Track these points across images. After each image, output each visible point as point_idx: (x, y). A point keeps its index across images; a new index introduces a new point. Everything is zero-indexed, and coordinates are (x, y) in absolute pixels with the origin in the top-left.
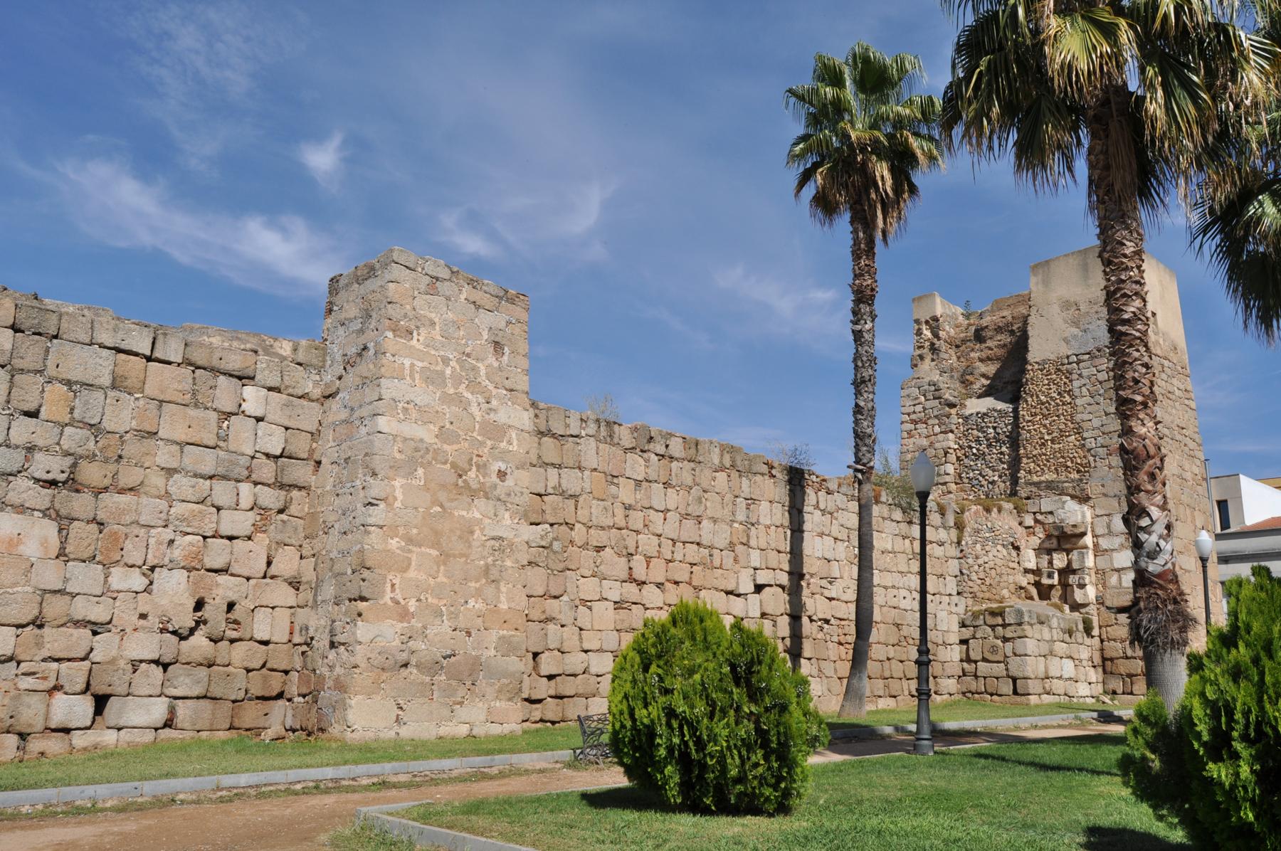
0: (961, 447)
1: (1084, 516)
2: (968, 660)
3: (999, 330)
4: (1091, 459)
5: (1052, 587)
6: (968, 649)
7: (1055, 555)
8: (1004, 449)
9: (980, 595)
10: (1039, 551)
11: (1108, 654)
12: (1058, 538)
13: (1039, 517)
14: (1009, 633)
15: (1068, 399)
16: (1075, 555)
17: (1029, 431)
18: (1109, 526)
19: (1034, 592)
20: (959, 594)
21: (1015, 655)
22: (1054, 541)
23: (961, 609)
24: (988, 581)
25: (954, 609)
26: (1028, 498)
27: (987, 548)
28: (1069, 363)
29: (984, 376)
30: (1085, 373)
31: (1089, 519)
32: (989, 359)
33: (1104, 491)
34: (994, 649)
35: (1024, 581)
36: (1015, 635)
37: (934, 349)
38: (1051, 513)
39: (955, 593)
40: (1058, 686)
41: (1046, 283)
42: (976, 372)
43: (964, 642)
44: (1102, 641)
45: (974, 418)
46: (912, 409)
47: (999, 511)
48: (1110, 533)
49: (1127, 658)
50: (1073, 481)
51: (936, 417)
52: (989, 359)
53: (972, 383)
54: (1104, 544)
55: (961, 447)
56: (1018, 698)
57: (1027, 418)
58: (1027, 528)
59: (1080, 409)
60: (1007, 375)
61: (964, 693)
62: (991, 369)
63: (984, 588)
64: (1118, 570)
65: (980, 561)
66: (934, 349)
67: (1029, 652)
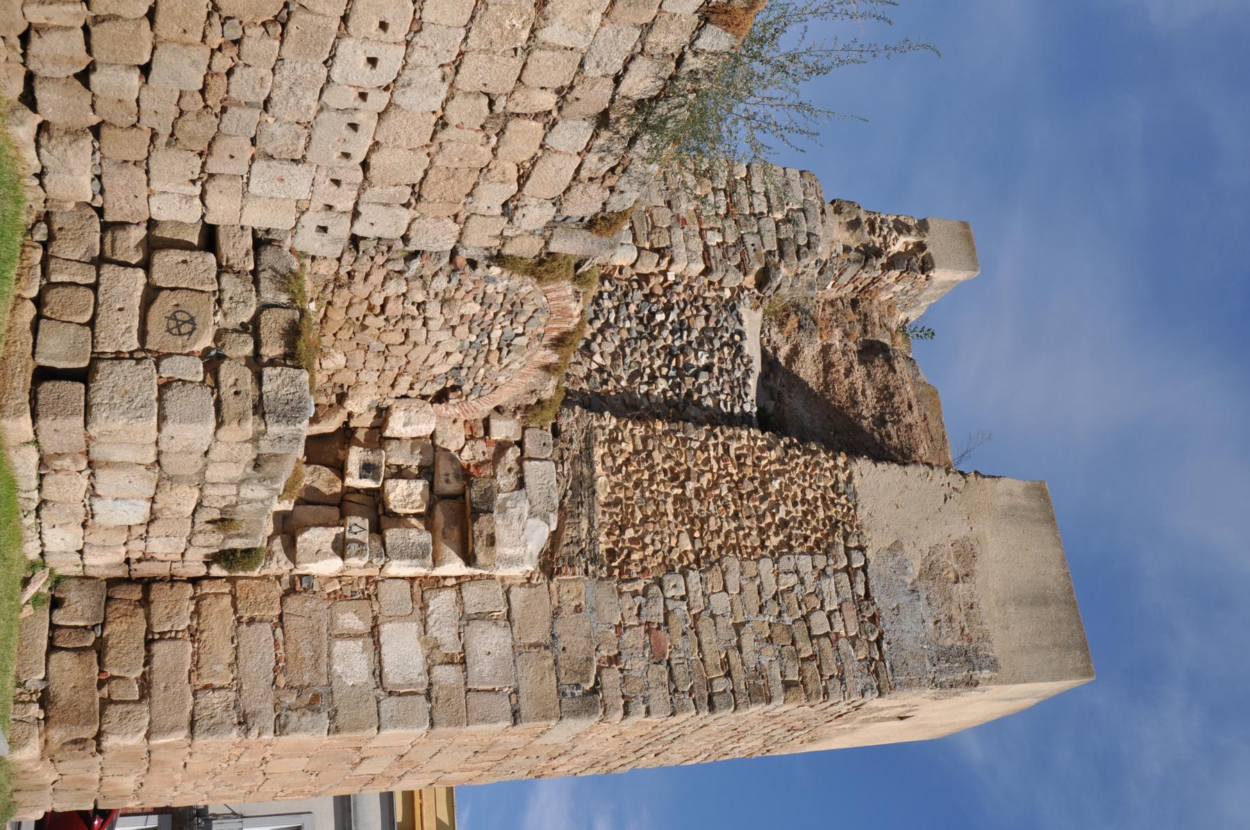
0: (669, 288)
1: (511, 561)
2: (153, 244)
3: (886, 394)
4: (639, 586)
5: (340, 469)
6: (187, 246)
7: (419, 486)
8: (662, 384)
9: (342, 298)
10: (430, 445)
11: (160, 594)
12: (459, 497)
13: (512, 455)
14: (233, 374)
15: (773, 541)
16: (418, 535)
17: (704, 447)
18: (480, 617)
19: (330, 425)
20: (355, 240)
21: (165, 386)
22: (453, 487)
23: (308, 241)
24: (374, 322)
25: (311, 220)
26: (556, 432)
27: (462, 330)
28: (848, 550)
29: (795, 352)
30: (828, 585)
31: (501, 572)
32: (828, 367)
33: (567, 610)
34: (183, 324)
35: (360, 408)
36: (226, 391)
37: (868, 254)
38: (521, 484)
39: (359, 229)
40: (68, 486)
41: (1011, 514)
42: (803, 337)
43: (210, 238)
44: (195, 581)
45: (732, 324)
46: (758, 187)
47: (547, 368)
48: (466, 619)
49: (149, 643)
50: (593, 541)
51: (741, 239)
52: (828, 367)
53: (782, 324)
54: (442, 603)
55: (669, 288)
56: (22, 382)
57: (734, 445)
58: (486, 423)
59: (750, 567)
60: (795, 403)
61: (47, 218)
62: (808, 370)
63: (358, 311)
64: (374, 632)
65: (433, 309)
66: (868, 254)
67: (169, 428)
